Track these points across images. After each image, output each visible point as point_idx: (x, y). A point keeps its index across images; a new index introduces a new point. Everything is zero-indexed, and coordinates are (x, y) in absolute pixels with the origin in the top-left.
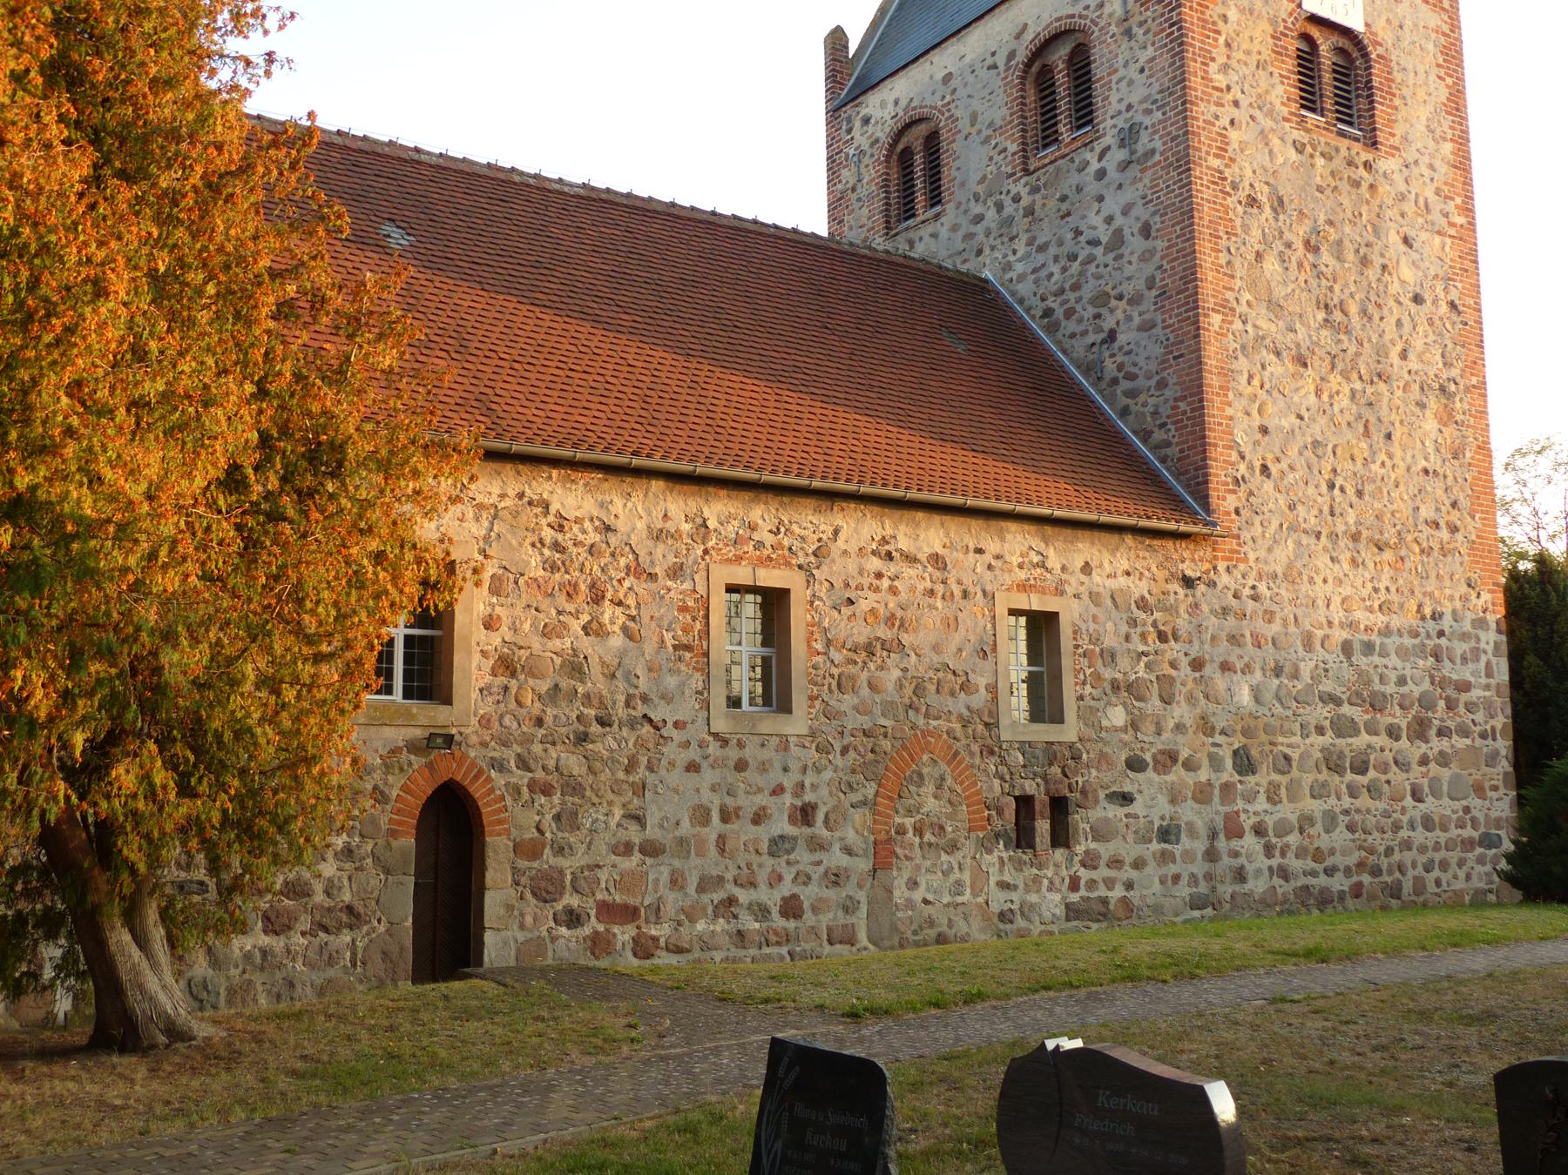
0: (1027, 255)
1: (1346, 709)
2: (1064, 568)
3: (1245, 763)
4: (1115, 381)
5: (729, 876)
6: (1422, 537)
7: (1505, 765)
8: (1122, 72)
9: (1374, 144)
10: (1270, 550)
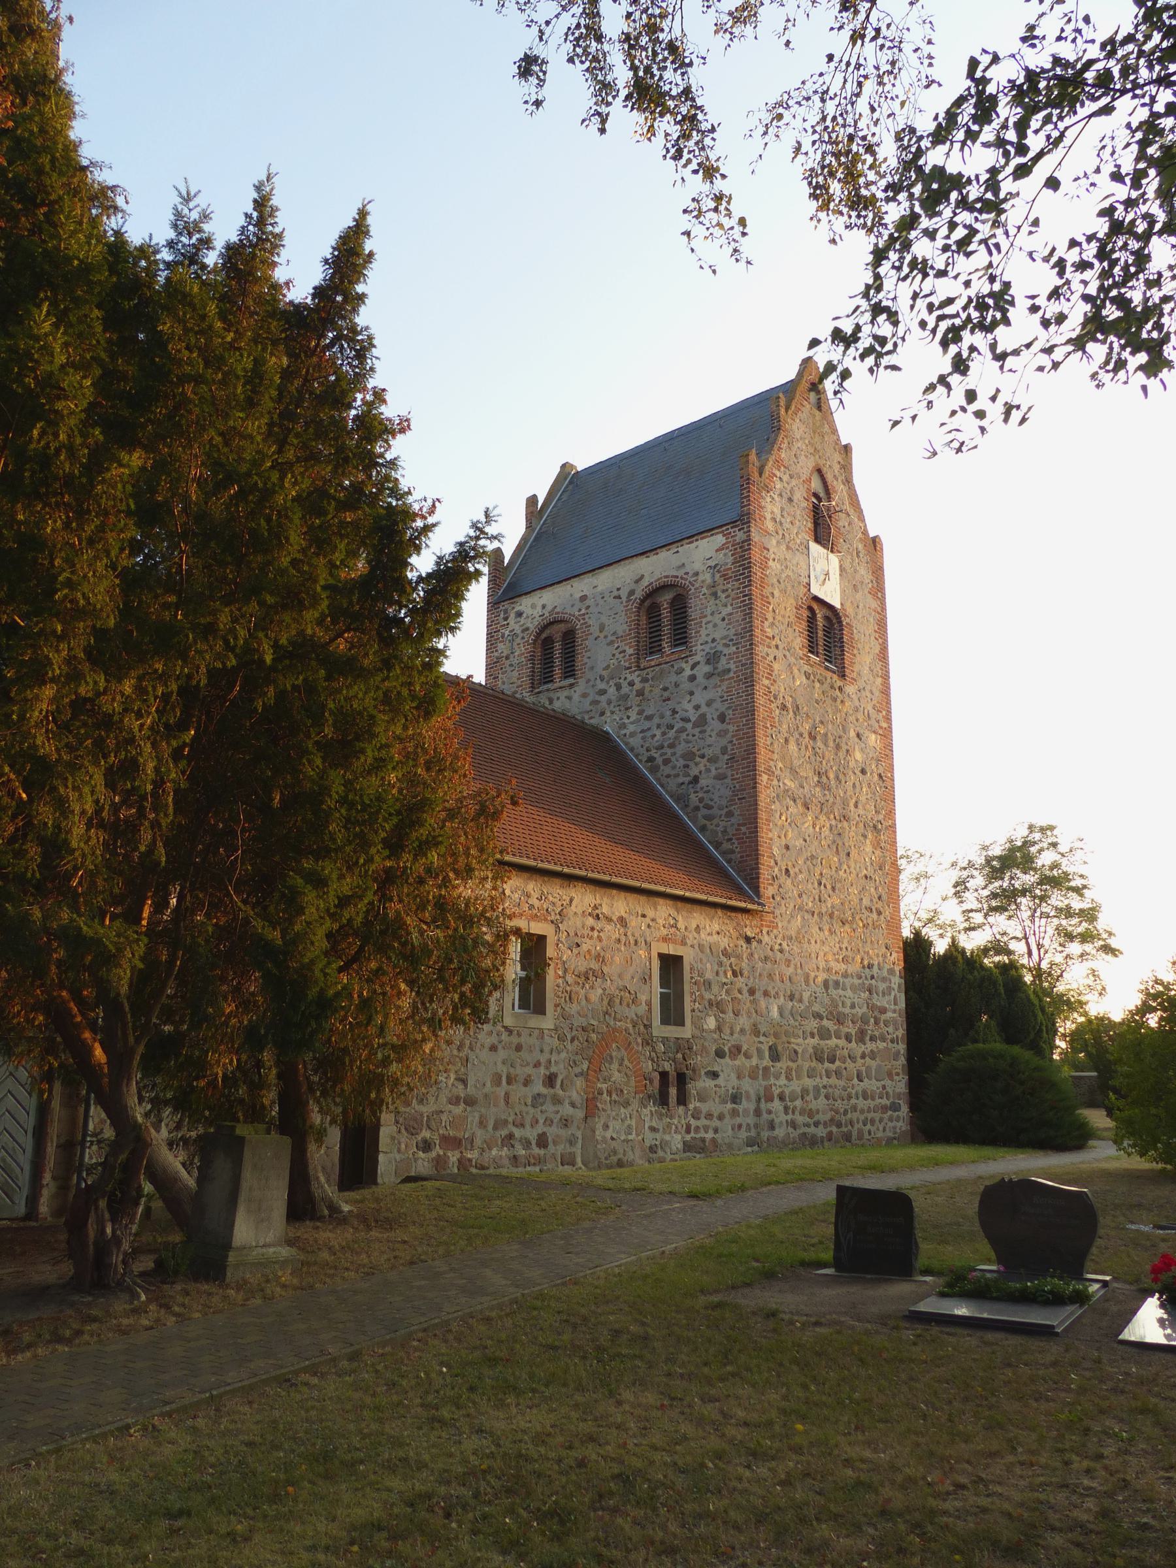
0: (638, 721)
1: (825, 1022)
2: (686, 928)
3: (775, 1056)
4: (697, 808)
5: (510, 1120)
6: (864, 917)
7: (902, 1060)
8: (709, 618)
9: (843, 676)
10: (789, 922)
